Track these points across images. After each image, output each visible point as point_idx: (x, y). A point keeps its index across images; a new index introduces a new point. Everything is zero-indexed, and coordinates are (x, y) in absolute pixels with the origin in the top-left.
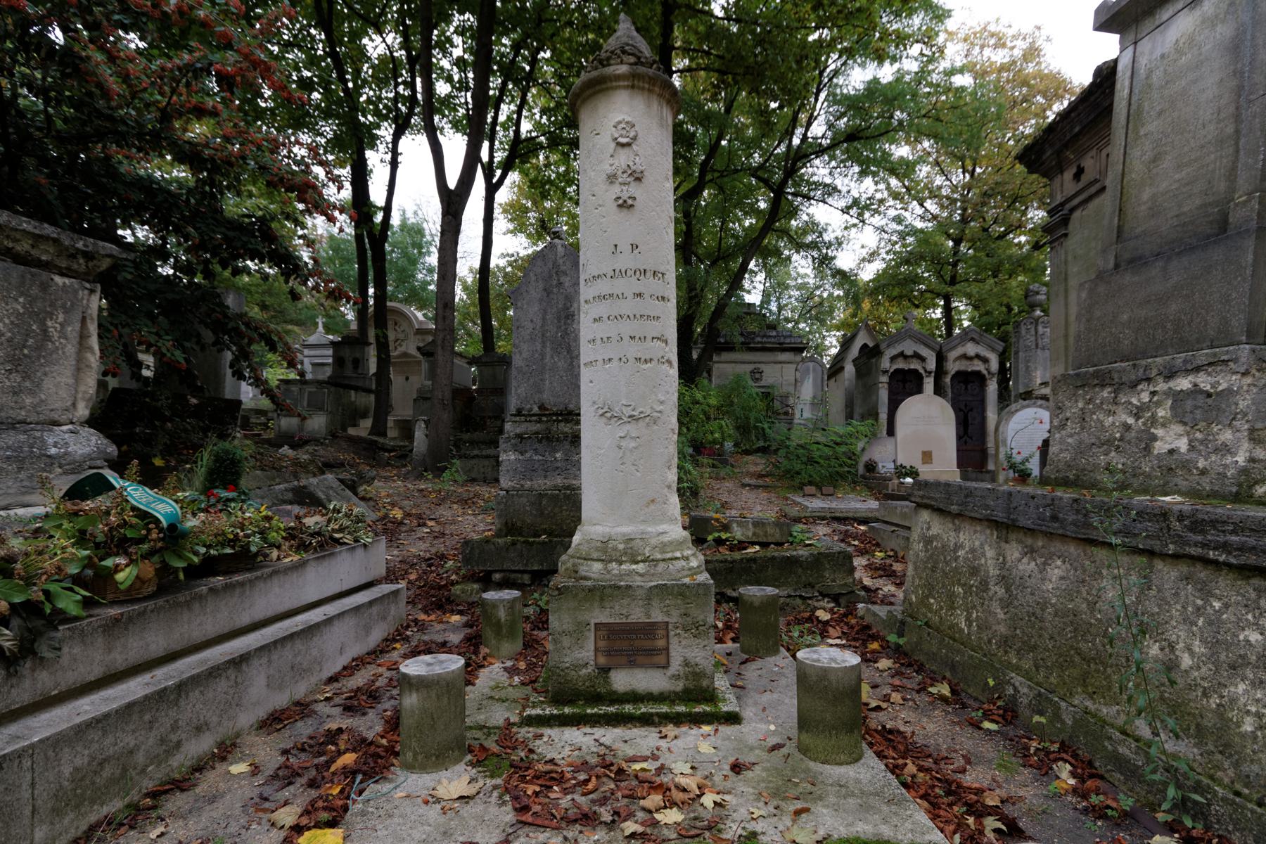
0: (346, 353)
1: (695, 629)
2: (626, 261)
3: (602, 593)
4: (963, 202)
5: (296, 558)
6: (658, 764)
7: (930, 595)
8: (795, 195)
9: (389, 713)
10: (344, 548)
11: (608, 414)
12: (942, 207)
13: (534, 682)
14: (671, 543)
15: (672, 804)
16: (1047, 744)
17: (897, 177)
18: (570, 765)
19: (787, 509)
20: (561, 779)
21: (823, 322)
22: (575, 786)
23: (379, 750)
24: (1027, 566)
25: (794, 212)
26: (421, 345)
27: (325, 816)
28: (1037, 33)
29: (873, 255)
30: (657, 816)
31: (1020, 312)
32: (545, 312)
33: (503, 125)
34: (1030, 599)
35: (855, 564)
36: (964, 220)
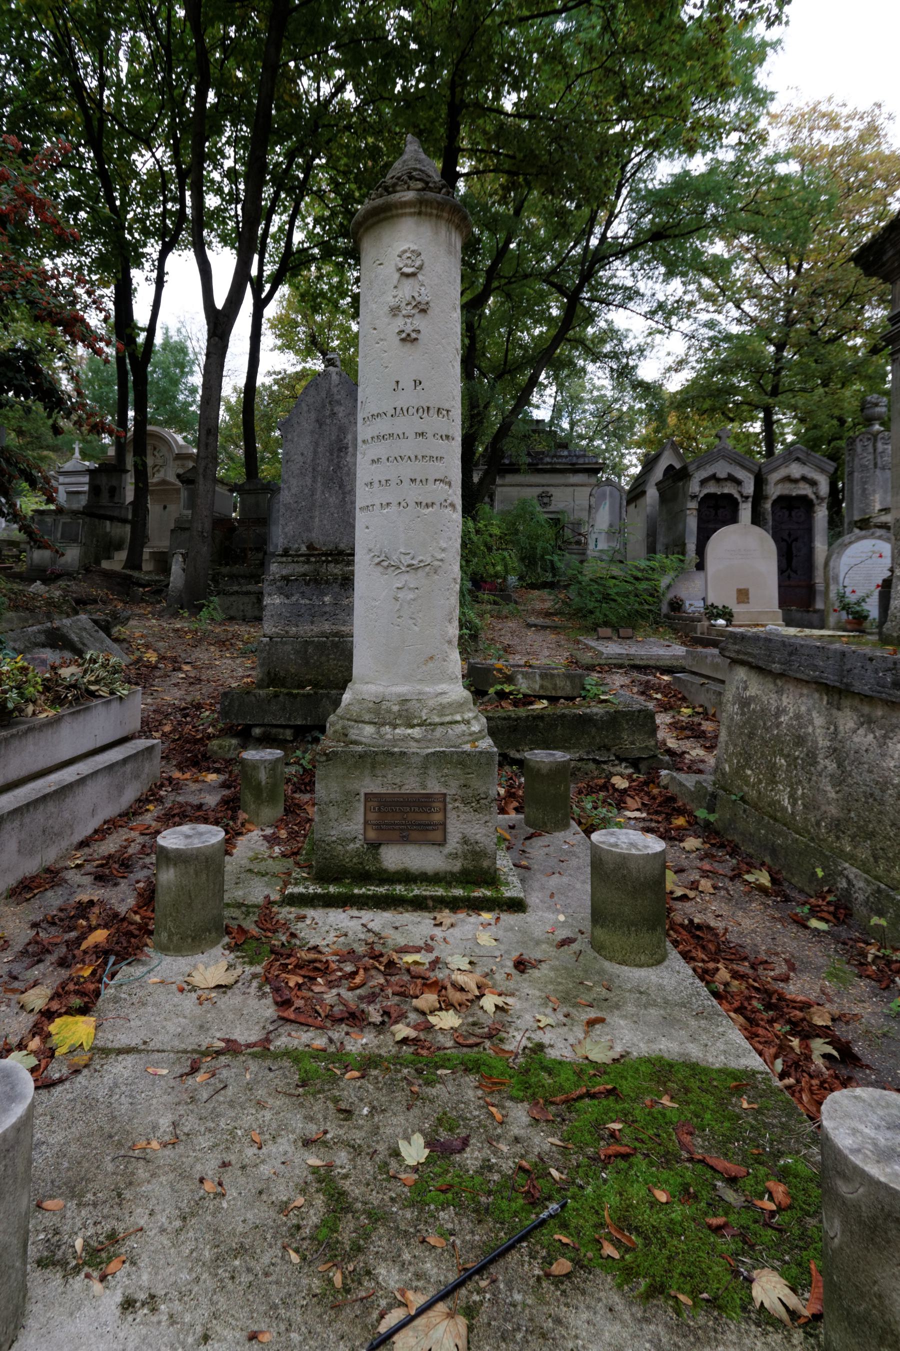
0: (103, 481)
1: (476, 802)
2: (408, 398)
3: (373, 760)
4: (787, 303)
5: (51, 713)
6: (431, 957)
7: (747, 765)
8: (591, 300)
9: (141, 885)
10: (100, 701)
11: (384, 563)
12: (762, 309)
13: (296, 854)
14: (450, 705)
15: (447, 1005)
16: (888, 952)
17: (709, 276)
18: (335, 954)
19: (579, 655)
20: (325, 970)
21: (621, 439)
22: (341, 978)
23: (132, 927)
24: (864, 739)
25: (590, 318)
26: (181, 471)
27: (76, 1001)
28: (877, 111)
29: (681, 364)
30: (432, 1019)
31: (855, 425)
32: (317, 444)
33: (274, 237)
34: (867, 777)
35: (658, 721)
36: (789, 322)
